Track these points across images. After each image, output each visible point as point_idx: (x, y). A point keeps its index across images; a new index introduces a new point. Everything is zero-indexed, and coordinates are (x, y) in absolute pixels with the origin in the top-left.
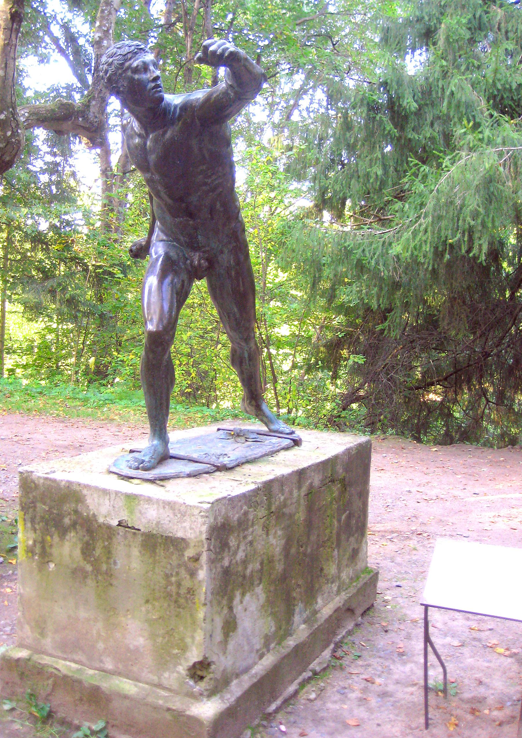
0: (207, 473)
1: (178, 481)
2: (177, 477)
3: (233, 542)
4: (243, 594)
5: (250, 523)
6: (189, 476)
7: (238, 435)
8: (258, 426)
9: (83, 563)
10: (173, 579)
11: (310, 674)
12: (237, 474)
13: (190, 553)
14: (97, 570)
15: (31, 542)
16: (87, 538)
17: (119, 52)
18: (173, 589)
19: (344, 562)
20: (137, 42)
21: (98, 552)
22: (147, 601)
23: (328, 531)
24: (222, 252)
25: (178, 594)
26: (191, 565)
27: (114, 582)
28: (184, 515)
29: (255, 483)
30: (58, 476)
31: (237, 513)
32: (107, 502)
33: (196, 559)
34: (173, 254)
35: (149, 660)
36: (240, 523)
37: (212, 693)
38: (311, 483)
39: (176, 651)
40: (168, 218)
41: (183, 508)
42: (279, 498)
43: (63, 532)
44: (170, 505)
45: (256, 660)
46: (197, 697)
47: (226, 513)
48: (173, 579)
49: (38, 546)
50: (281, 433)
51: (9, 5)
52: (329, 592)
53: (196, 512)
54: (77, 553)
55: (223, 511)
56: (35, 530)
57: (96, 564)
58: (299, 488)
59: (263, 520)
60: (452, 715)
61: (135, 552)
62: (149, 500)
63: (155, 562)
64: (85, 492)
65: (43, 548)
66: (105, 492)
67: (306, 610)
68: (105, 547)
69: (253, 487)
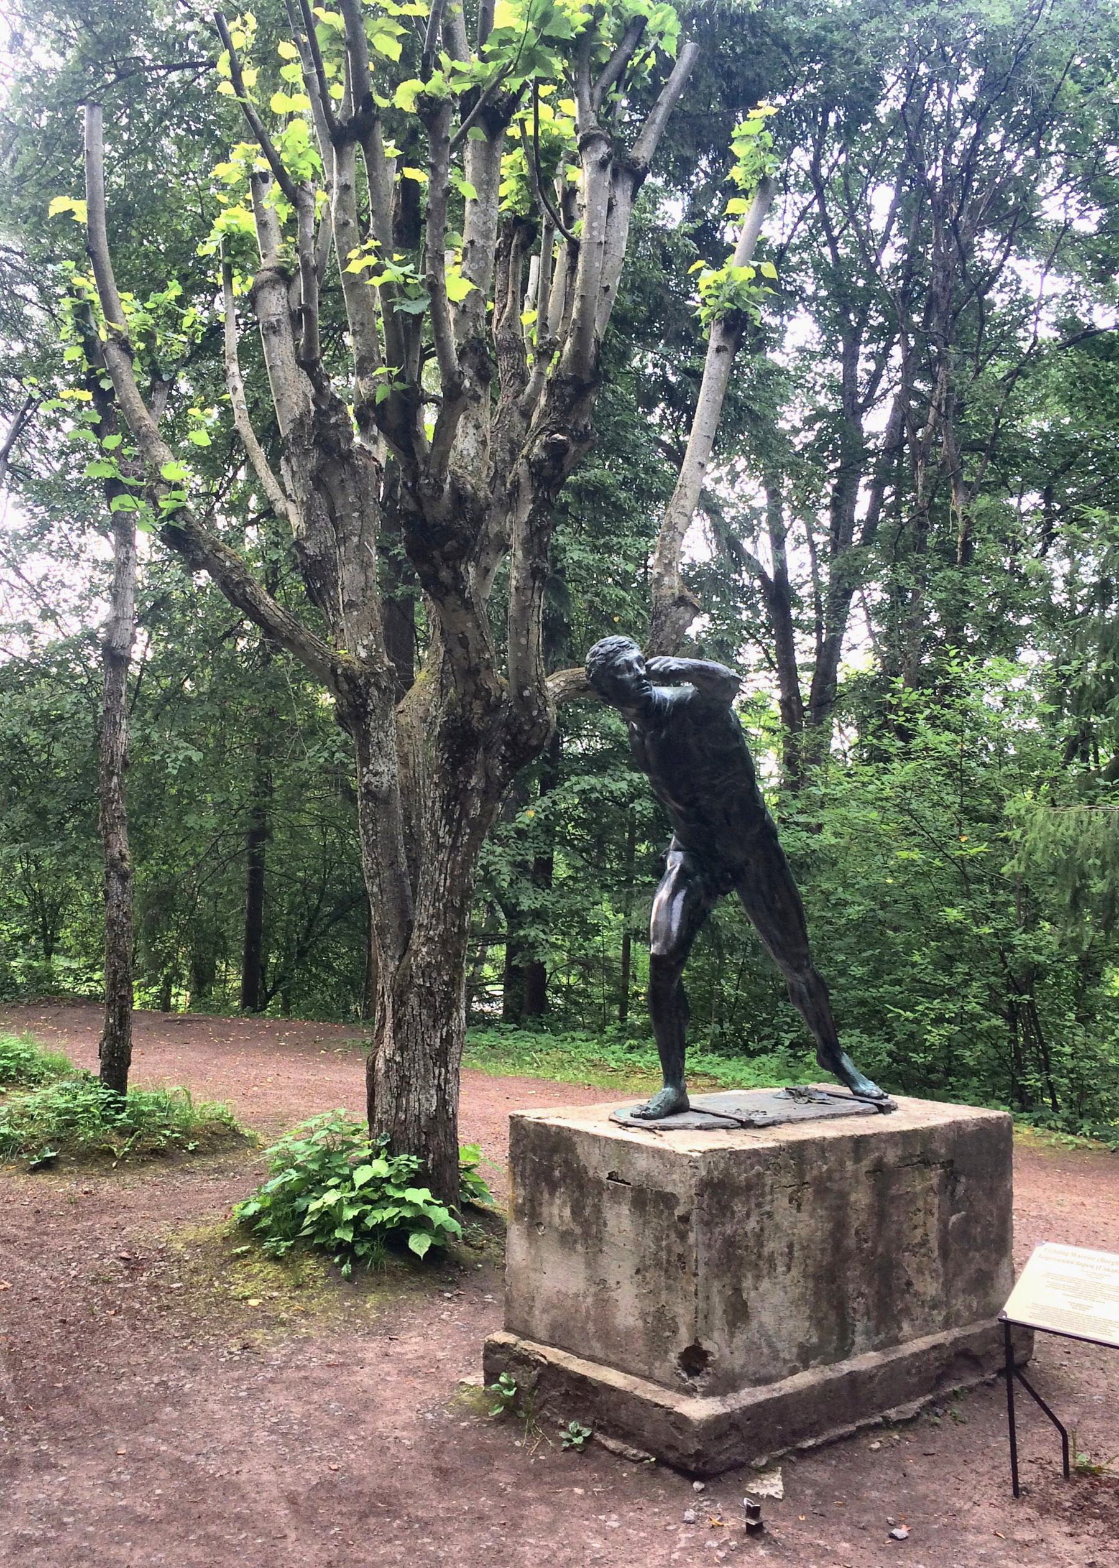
0: (726, 1128)
1: (683, 1132)
2: (684, 1127)
3: (739, 1207)
4: (758, 1277)
5: (767, 1189)
6: (699, 1128)
7: (801, 1095)
8: (846, 1091)
9: (572, 1225)
10: (664, 1243)
11: (879, 1419)
12: (762, 1134)
13: (679, 1211)
14: (586, 1235)
15: (520, 1201)
16: (576, 1195)
17: (602, 651)
18: (663, 1255)
19: (959, 1284)
20: (622, 638)
21: (587, 1211)
22: (638, 1272)
23: (919, 1232)
24: (747, 863)
25: (668, 1261)
26: (681, 1226)
27: (605, 1249)
28: (672, 1166)
29: (777, 1140)
30: (551, 1121)
31: (746, 1171)
32: (597, 1151)
33: (685, 1219)
34: (688, 866)
35: (639, 1345)
36: (749, 1187)
37: (708, 1393)
38: (880, 1159)
39: (667, 1334)
40: (682, 822)
41: (672, 1157)
42: (820, 1167)
43: (553, 1187)
44: (658, 1153)
45: (785, 1373)
46: (690, 1392)
47: (727, 1169)
48: (664, 1243)
49: (528, 1205)
50: (868, 1096)
51: (990, 300)
52: (925, 1320)
53: (685, 1161)
54: (567, 1212)
55: (722, 1165)
56: (524, 1185)
57: (585, 1224)
58: (857, 1160)
59: (789, 1190)
60: (106, 837)
61: (625, 1210)
62: (638, 1147)
63: (646, 1223)
64: (575, 1139)
65: (533, 1207)
66: (595, 1138)
67: (877, 1334)
68: (594, 1205)
69: (771, 1144)
